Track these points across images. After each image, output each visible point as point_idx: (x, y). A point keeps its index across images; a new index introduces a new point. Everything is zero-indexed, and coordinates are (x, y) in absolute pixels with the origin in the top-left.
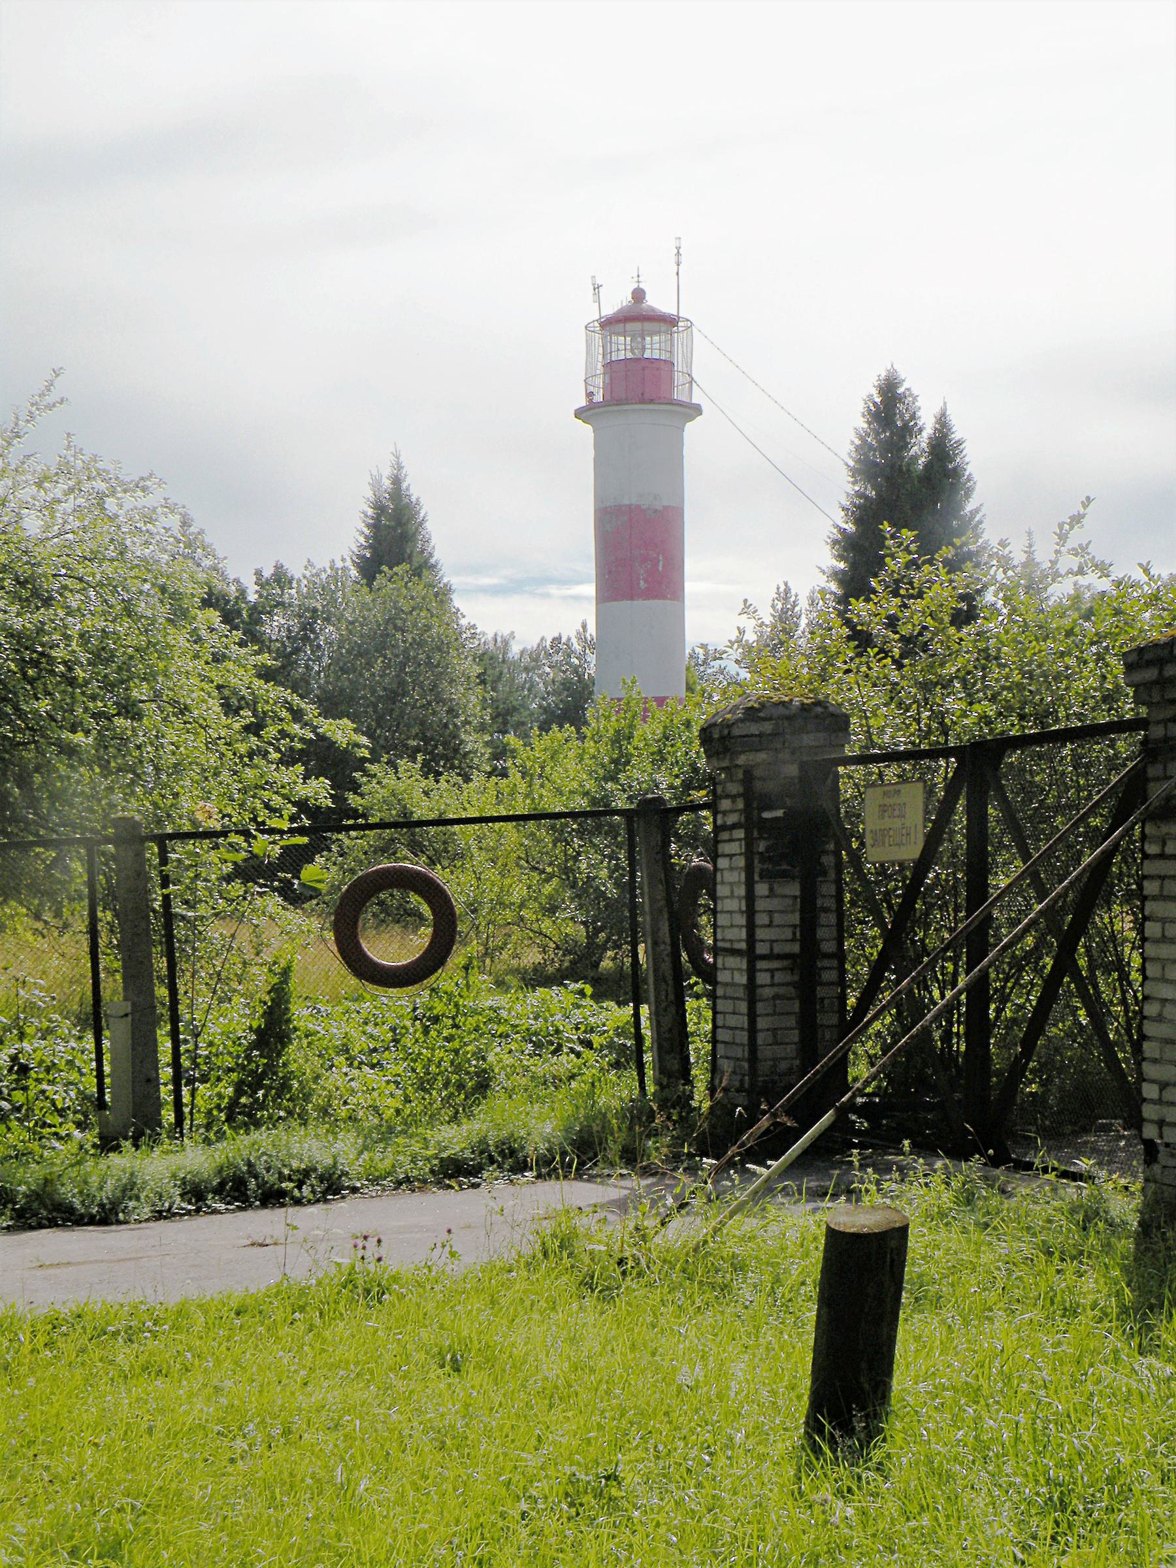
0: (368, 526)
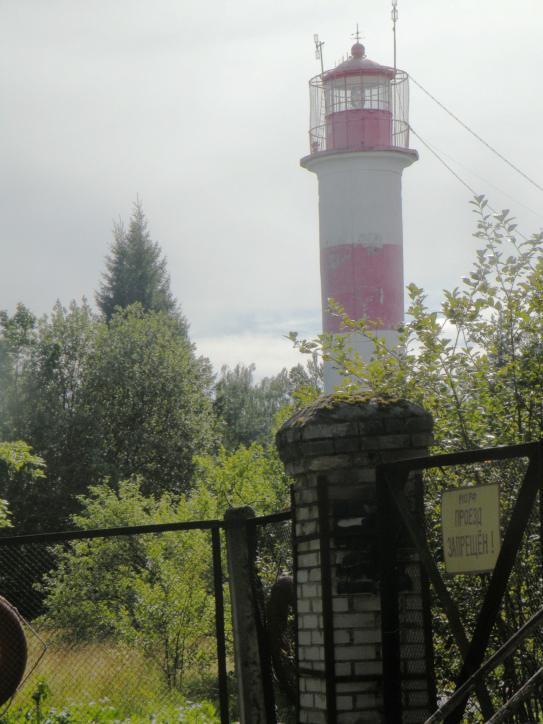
0: (110, 269)
